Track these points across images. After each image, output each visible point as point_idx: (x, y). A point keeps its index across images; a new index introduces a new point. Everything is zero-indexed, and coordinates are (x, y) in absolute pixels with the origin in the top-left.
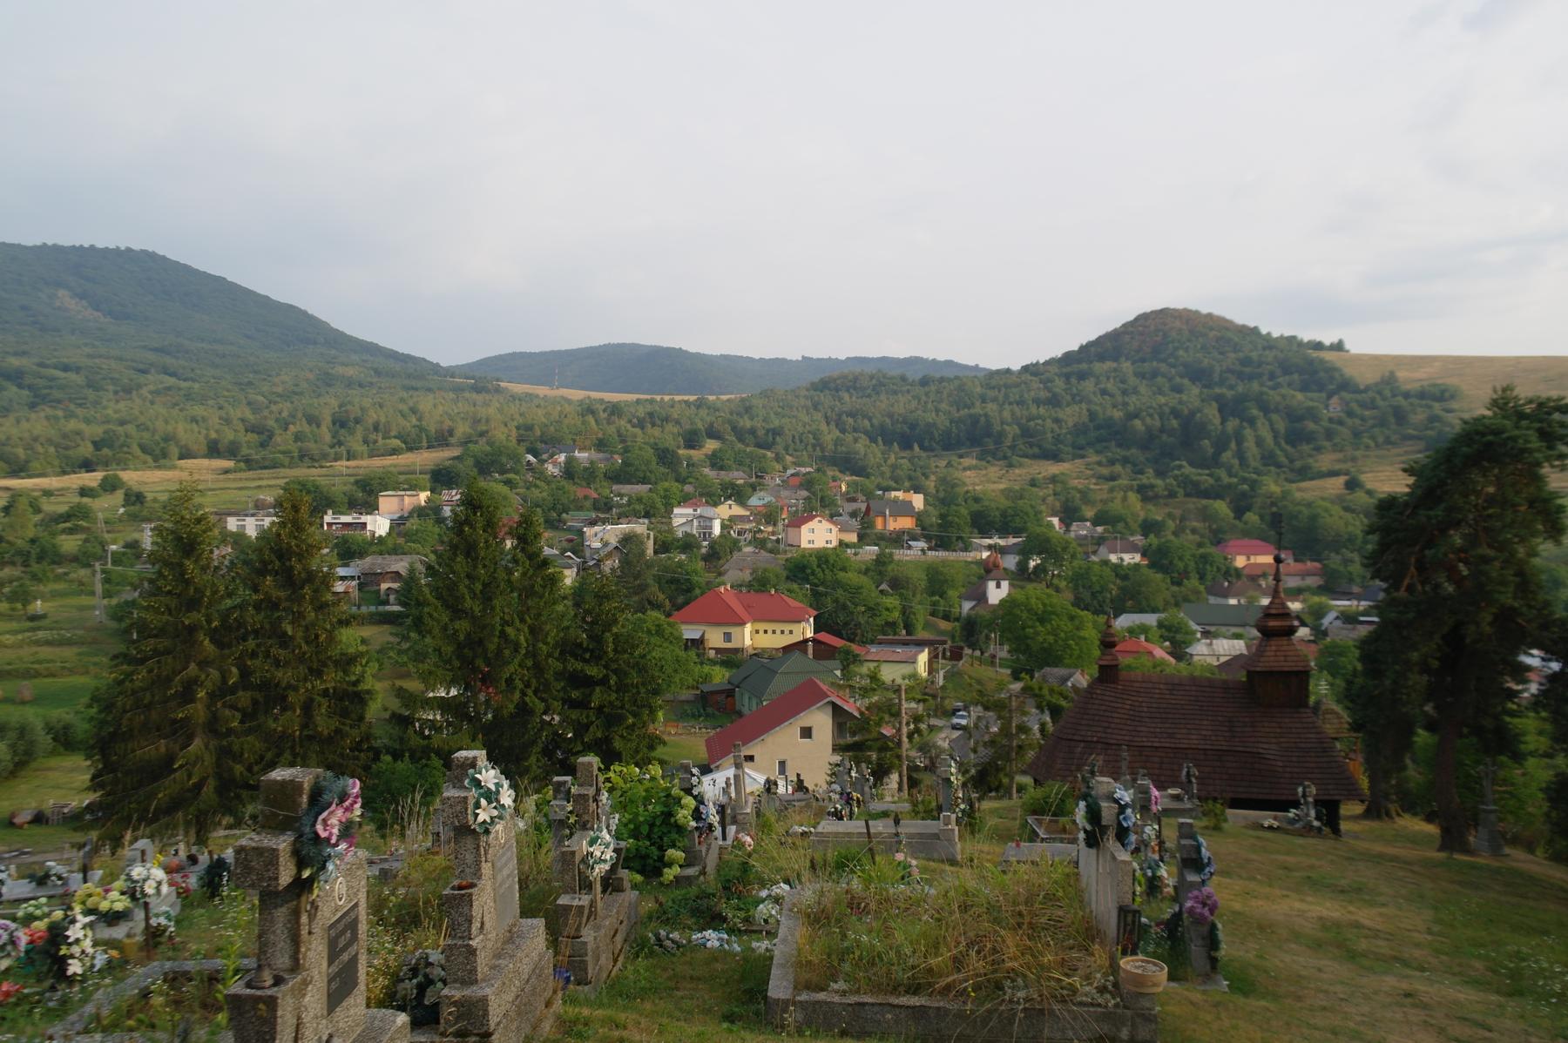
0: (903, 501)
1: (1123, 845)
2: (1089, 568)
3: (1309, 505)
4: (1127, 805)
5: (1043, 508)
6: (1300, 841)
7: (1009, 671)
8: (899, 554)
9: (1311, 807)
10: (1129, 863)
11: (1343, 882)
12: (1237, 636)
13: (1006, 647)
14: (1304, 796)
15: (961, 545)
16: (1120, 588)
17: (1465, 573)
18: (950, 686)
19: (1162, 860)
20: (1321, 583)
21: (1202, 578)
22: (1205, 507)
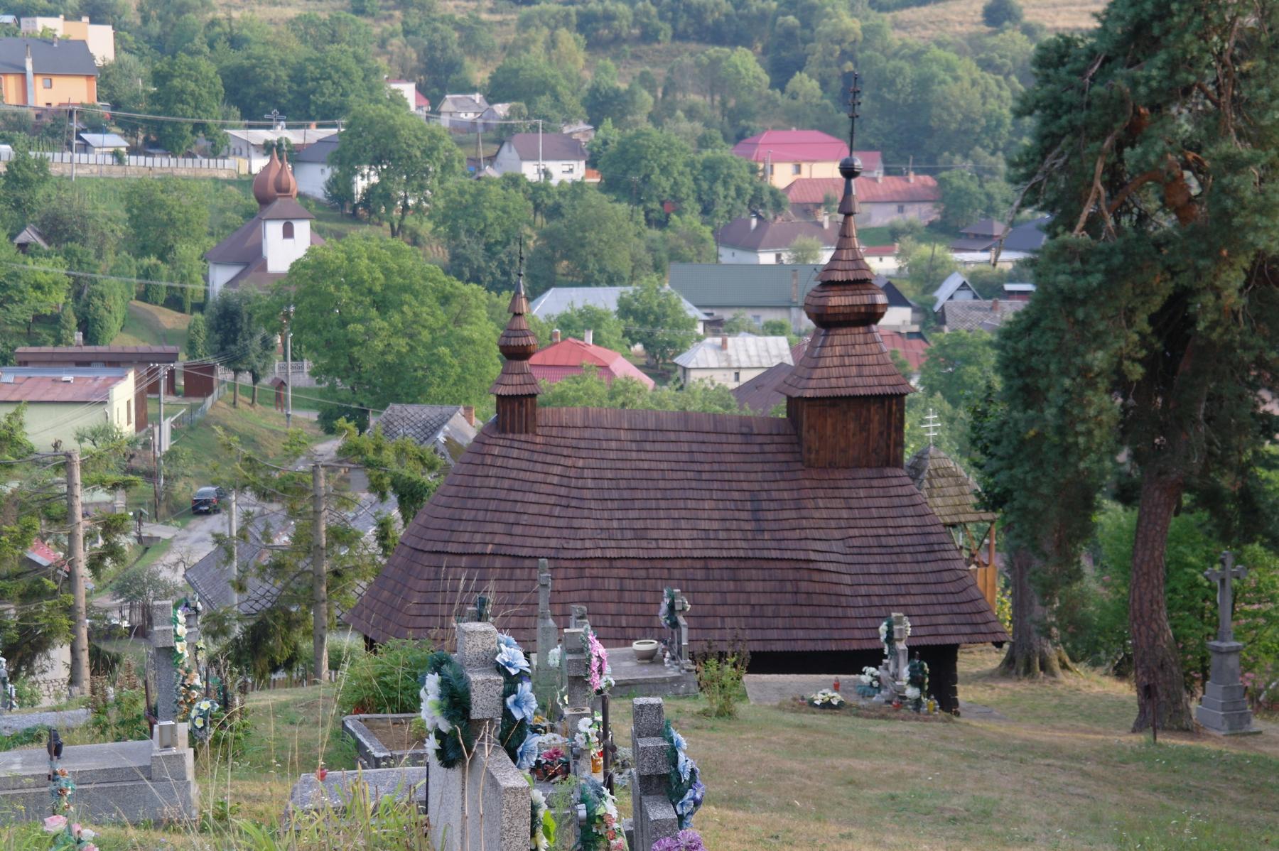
0: (66, 42)
1: (514, 758)
2: (480, 193)
3: (916, 57)
4: (522, 675)
5: (382, 62)
6: (881, 727)
7: (314, 416)
8: (60, 162)
9: (903, 660)
10: (525, 792)
11: (955, 802)
12: (775, 329)
13: (307, 365)
14: (890, 639)
15: (202, 142)
16: (545, 235)
17: (1195, 190)
18: (186, 451)
19: (609, 784)
20: (935, 217)
21: (707, 210)
22: (715, 62)
